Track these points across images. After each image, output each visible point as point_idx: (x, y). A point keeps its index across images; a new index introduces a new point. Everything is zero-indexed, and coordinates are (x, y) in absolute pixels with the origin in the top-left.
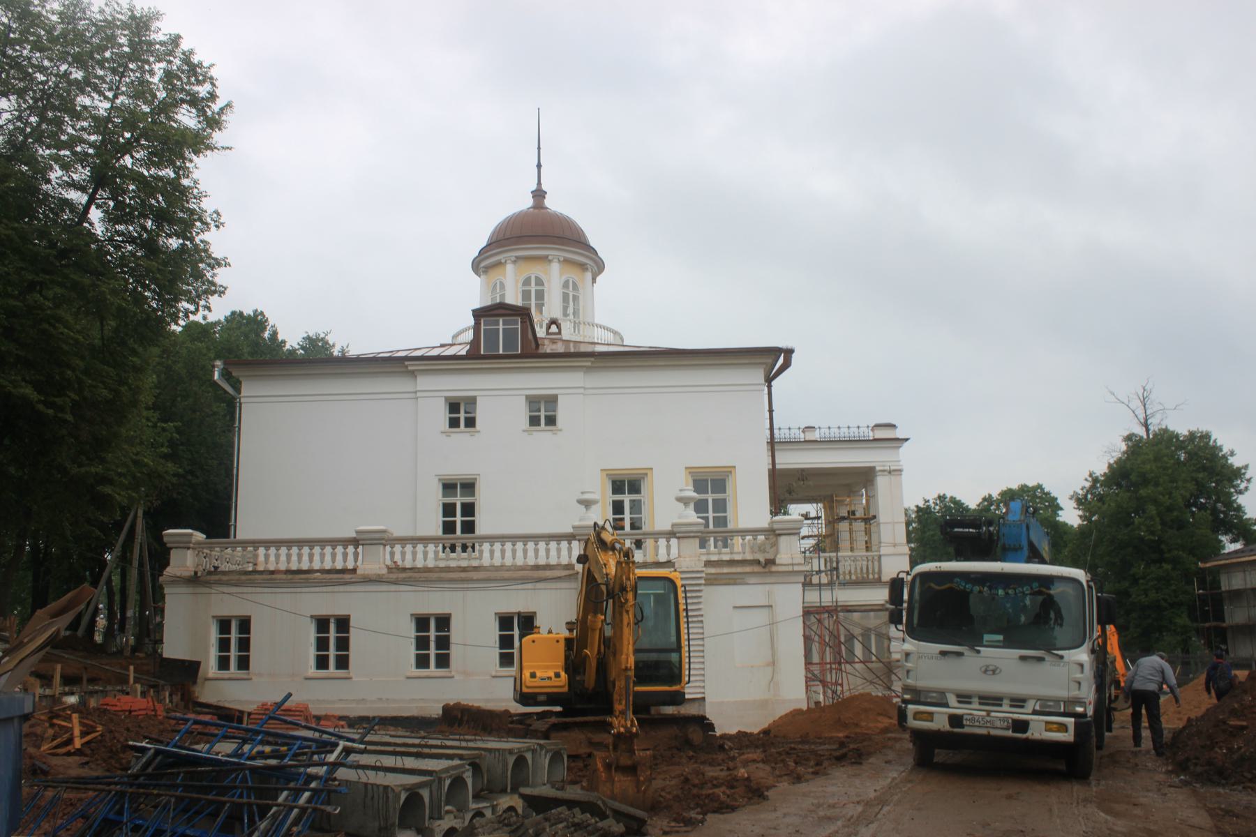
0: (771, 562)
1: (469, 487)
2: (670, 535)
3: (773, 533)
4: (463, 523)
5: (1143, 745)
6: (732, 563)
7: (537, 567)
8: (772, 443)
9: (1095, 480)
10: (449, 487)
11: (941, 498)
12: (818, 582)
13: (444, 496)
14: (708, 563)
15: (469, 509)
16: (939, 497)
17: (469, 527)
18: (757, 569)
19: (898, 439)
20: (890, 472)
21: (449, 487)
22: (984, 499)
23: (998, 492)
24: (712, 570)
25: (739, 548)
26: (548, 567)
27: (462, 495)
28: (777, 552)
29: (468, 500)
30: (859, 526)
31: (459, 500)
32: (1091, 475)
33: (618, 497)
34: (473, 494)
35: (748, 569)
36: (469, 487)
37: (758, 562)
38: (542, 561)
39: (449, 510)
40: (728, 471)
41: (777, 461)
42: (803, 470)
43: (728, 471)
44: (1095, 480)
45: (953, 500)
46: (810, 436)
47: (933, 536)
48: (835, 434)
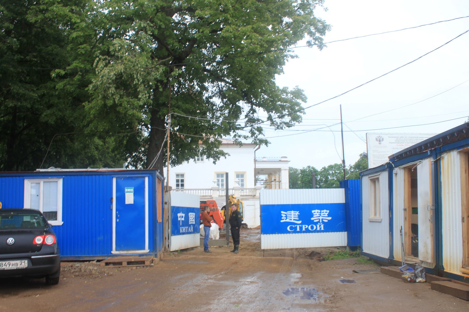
0: (255, 196)
1: (182, 175)
2: (233, 189)
3: (255, 189)
4: (181, 184)
5: (401, 261)
6: (246, 196)
7: (203, 196)
8: (255, 161)
9: (351, 167)
10: (178, 175)
11: (309, 167)
12: (278, 180)
13: (176, 177)
14: (241, 196)
15: (182, 181)
16: (308, 167)
17: (182, 185)
18: (252, 197)
19: (287, 161)
20: (285, 170)
21: (178, 175)
22: (323, 168)
23: (328, 166)
24: (242, 197)
25: (247, 193)
26: (206, 196)
27: (181, 177)
28: (256, 193)
29: (182, 179)
30: (277, 183)
31: (180, 179)
32: (350, 165)
33: (218, 178)
34: (183, 177)
35: (250, 197)
36: (182, 175)
37: (252, 196)
38: (204, 195)
39: (177, 181)
40: (245, 172)
41: (256, 166)
42: (262, 169)
43: (245, 172)
44: (351, 167)
45: (313, 168)
46: (264, 160)
47: (305, 180)
48: (271, 159)
